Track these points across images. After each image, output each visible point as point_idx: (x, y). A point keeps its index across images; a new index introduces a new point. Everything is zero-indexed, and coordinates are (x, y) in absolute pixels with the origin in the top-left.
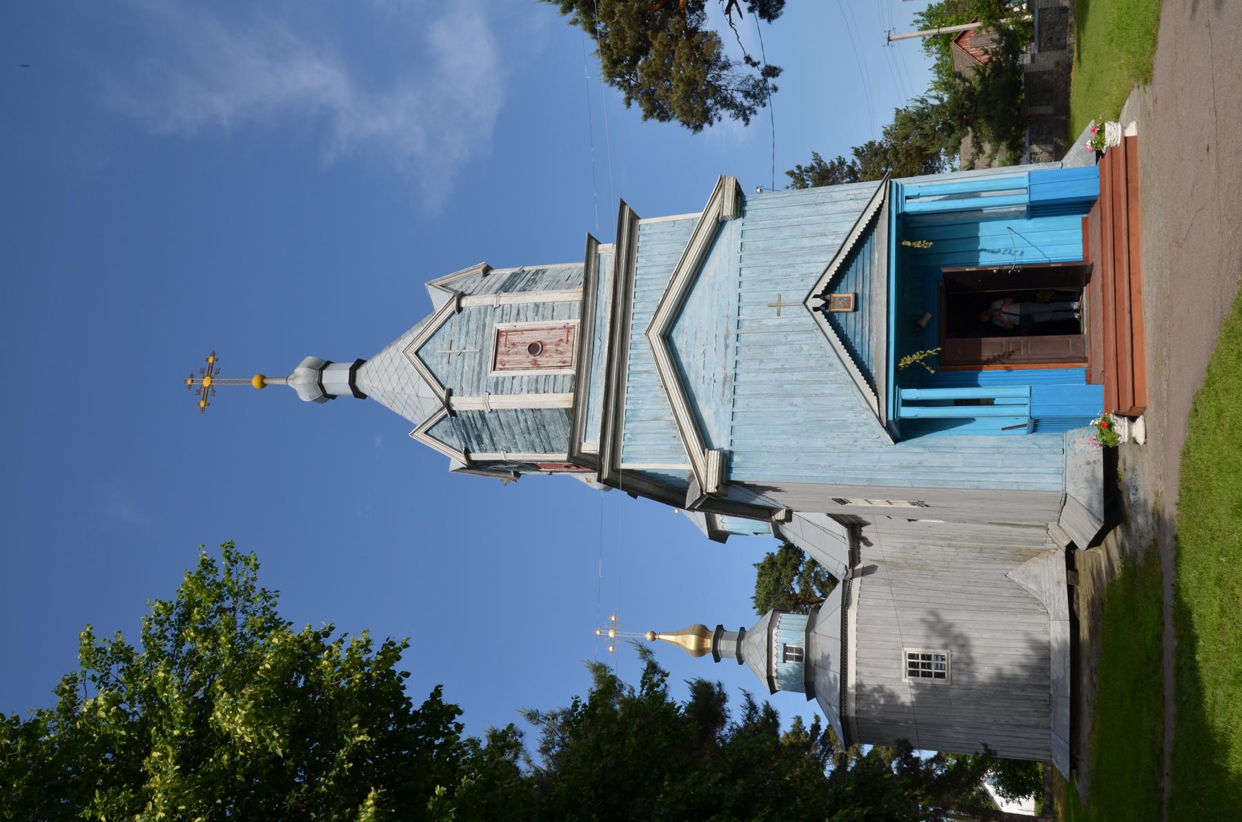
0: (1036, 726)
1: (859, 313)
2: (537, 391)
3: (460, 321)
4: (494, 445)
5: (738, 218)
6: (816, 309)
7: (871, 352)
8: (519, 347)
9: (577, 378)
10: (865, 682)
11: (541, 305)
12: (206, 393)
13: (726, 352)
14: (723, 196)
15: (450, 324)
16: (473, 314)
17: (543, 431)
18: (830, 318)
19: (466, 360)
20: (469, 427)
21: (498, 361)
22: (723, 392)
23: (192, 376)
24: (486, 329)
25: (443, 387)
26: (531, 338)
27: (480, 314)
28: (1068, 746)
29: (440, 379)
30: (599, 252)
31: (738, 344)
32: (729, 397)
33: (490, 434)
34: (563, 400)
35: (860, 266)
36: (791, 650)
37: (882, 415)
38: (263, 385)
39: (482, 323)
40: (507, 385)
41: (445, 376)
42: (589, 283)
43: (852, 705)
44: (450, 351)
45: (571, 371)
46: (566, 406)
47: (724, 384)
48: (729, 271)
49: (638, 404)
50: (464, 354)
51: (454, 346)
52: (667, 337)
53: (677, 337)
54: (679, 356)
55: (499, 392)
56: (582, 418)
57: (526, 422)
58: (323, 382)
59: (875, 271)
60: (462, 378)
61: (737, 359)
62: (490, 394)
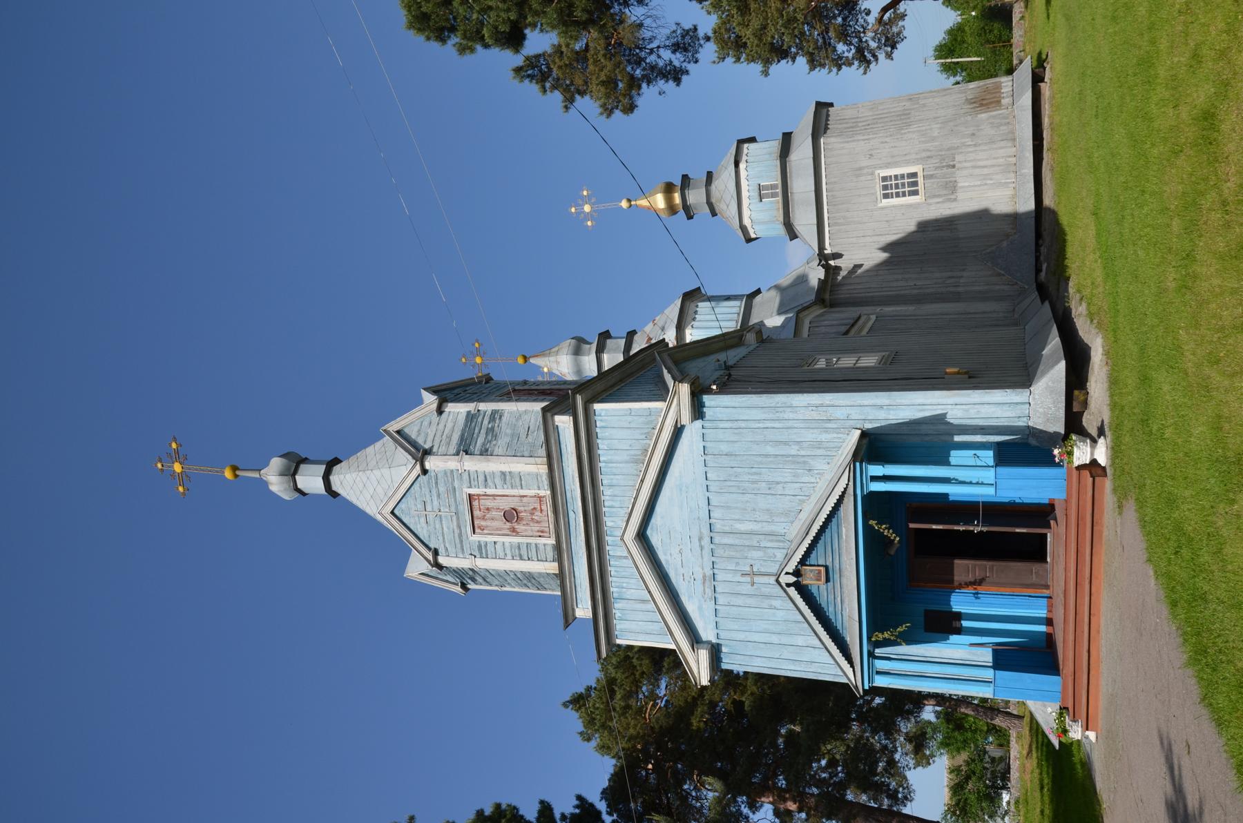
1: (830, 584)
2: (521, 558)
5: (697, 419)
6: (788, 585)
7: (844, 621)
9: (558, 548)
11: (508, 474)
12: (183, 478)
13: (702, 554)
15: (418, 485)
19: (444, 522)
21: (476, 525)
22: (704, 590)
24: (457, 493)
26: (506, 504)
29: (422, 539)
30: (556, 424)
31: (714, 559)
32: (710, 595)
36: (766, 188)
37: (858, 684)
38: (236, 476)
40: (490, 548)
41: (426, 536)
44: (426, 513)
48: (694, 473)
53: (652, 535)
54: (656, 553)
55: (484, 555)
56: (571, 587)
59: (843, 545)
60: (444, 538)
62: (475, 557)
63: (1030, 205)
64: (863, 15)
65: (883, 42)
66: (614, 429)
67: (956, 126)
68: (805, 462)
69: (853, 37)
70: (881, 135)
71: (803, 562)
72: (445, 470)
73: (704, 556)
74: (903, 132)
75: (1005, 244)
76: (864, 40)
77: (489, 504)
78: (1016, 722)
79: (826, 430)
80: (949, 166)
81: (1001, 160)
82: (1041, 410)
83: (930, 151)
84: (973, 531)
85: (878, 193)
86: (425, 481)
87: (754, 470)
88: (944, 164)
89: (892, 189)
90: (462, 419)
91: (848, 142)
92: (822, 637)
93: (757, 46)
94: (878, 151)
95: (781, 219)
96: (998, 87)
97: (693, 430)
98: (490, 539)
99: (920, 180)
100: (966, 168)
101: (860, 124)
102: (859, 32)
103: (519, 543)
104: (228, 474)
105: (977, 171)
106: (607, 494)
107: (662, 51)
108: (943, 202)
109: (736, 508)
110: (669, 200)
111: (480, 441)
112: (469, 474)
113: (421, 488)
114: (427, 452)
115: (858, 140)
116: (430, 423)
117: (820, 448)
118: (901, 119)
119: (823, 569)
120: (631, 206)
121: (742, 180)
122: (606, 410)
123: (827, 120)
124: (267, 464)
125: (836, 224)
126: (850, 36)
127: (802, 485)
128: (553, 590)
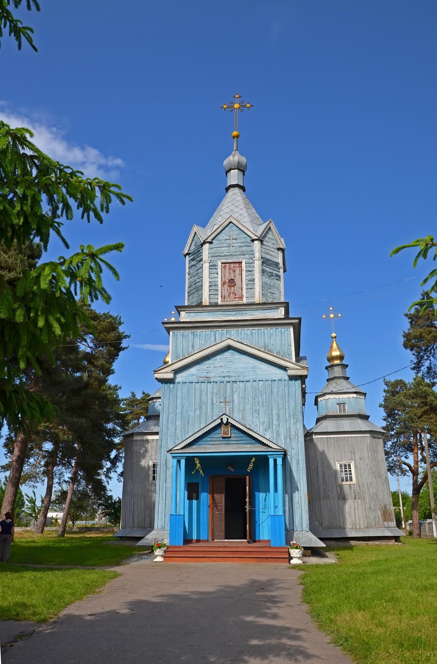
0: (133, 522)
1: (221, 439)
2: (210, 286)
3: (247, 242)
4: (191, 267)
6: (222, 419)
7: (203, 445)
8: (233, 274)
9: (216, 305)
10: (149, 444)
12: (231, 107)
14: (298, 369)
15: (246, 237)
16: (251, 248)
17: (195, 291)
18: (218, 426)
19: (227, 248)
20: (198, 254)
23: (240, 97)
25: (213, 240)
26: (237, 280)
27: (251, 252)
28: (124, 536)
29: (218, 236)
30: (280, 308)
31: (219, 382)
32: (200, 380)
33: (195, 265)
34: (206, 301)
35: (244, 439)
36: (344, 407)
38: (234, 137)
39: (246, 253)
40: (214, 271)
41: (219, 239)
42: (263, 305)
43: (139, 438)
44: (231, 239)
45: (220, 302)
46: (203, 302)
47: (206, 377)
49: (200, 337)
50: (230, 247)
51: (234, 241)
52: (229, 348)
53: (230, 353)
54: (220, 354)
55: (210, 267)
57: (199, 282)
58: (232, 171)
59: (242, 446)
60: (218, 247)
61: (218, 383)
62: (210, 263)
63: (351, 534)
64: (405, 455)
65: (391, 465)
66: (280, 337)
67: (375, 500)
68: (269, 428)
69: (394, 450)
70: (371, 464)
71: (233, 426)
72: (254, 251)
73: (220, 378)
74: (372, 475)
75: (317, 523)
76: (392, 455)
77: (237, 272)
78: (40, 530)
79: (285, 438)
80: (355, 496)
81: (358, 521)
82: (300, 536)
83: (363, 487)
84: (246, 505)
85: (343, 462)
86: (247, 241)
87: (265, 403)
88: (356, 494)
89: (345, 469)
90: (276, 260)
91: (367, 448)
92: (196, 434)
93: (395, 402)
94: (363, 463)
95: (329, 414)
96: (391, 520)
97: (283, 375)
98: (219, 271)
99: (349, 483)
100: (355, 505)
101: (375, 454)
102: (397, 453)
103: (218, 285)
104: (235, 133)
105: (353, 510)
106: (248, 331)
107: (428, 361)
108: (338, 493)
109: (245, 394)
110: (336, 358)
111: (267, 269)
112: (252, 263)
113: (244, 238)
114: (262, 241)
115: (368, 453)
116: (274, 244)
117: (277, 435)
118: (377, 474)
119: (229, 435)
120: (333, 338)
121: (348, 395)
122: (290, 333)
123: (377, 438)
124: (242, 154)
125: (327, 441)
126: (394, 448)
127: (258, 426)
128: (188, 300)
